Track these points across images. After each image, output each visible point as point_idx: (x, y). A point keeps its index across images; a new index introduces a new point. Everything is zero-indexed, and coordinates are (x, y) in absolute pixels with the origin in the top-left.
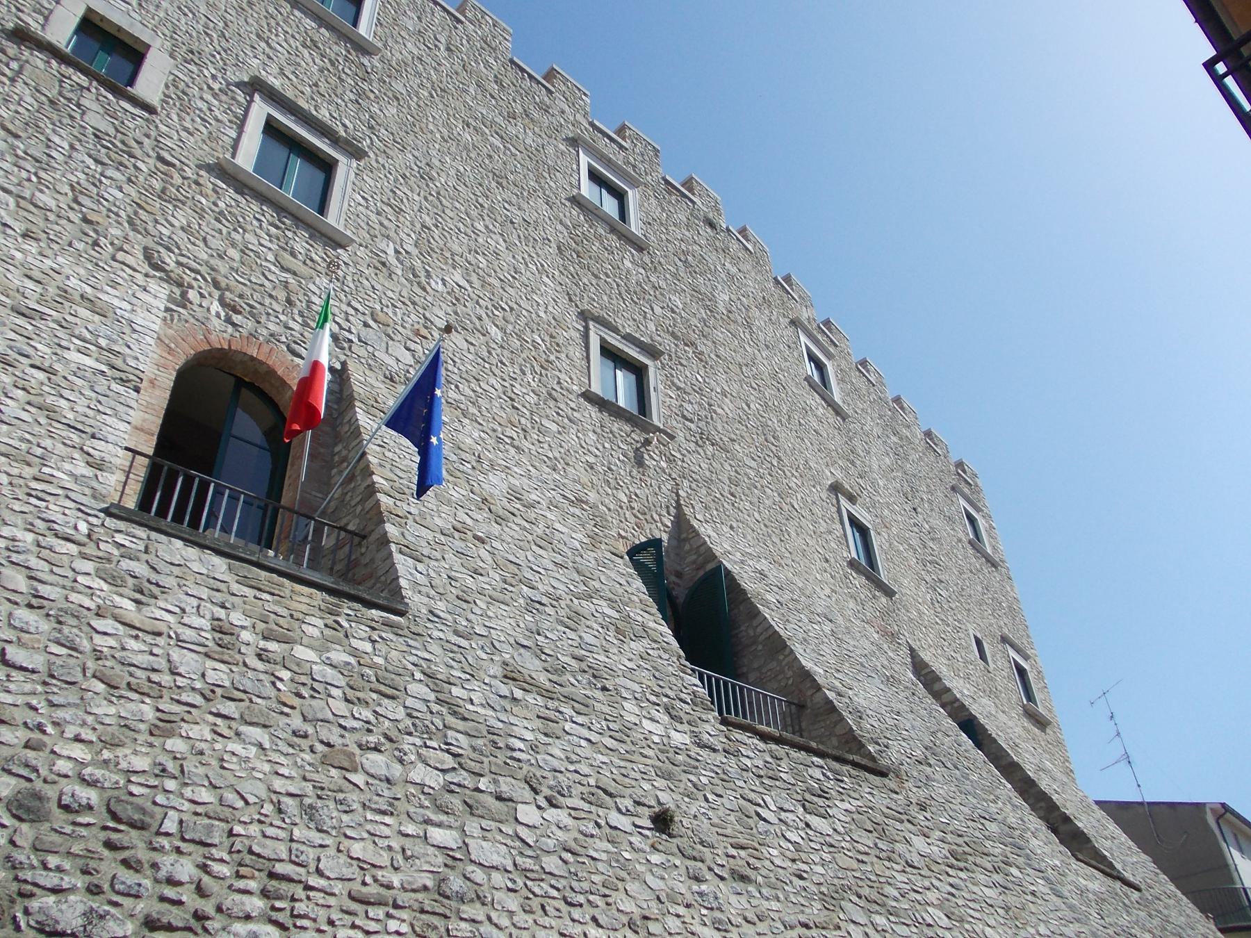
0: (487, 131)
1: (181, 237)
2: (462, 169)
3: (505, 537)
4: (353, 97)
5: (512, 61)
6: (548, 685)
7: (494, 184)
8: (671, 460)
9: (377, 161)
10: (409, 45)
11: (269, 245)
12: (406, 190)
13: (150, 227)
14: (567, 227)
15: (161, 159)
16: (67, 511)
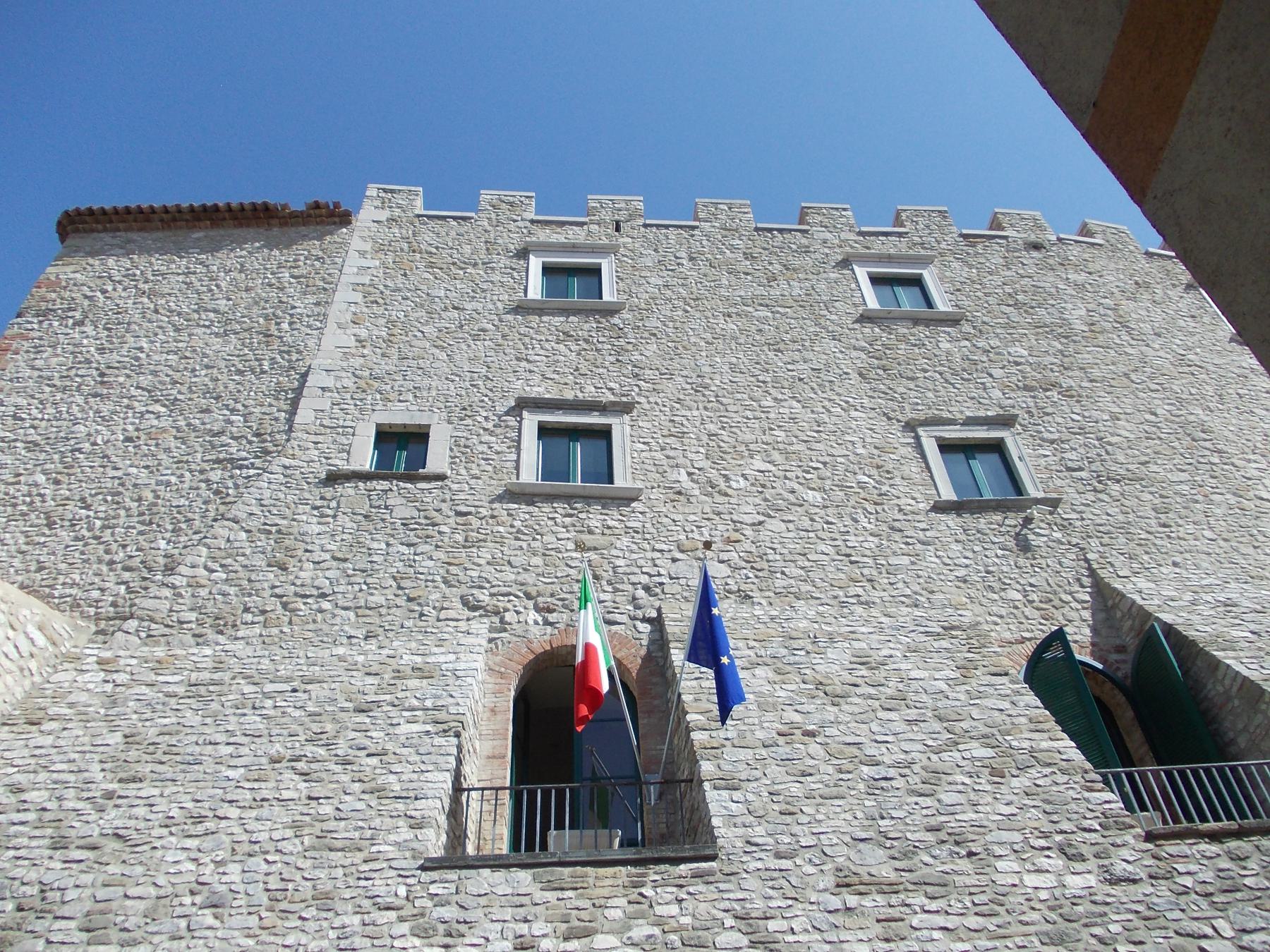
0: (750, 309)
1: (489, 572)
2: (734, 360)
3: (842, 717)
4: (612, 359)
5: (757, 229)
6: (893, 876)
7: (771, 354)
8: (1065, 526)
9: (649, 402)
10: (652, 280)
11: (568, 535)
12: (684, 412)
13: (462, 577)
14: (862, 349)
15: (459, 514)
16: (389, 882)
